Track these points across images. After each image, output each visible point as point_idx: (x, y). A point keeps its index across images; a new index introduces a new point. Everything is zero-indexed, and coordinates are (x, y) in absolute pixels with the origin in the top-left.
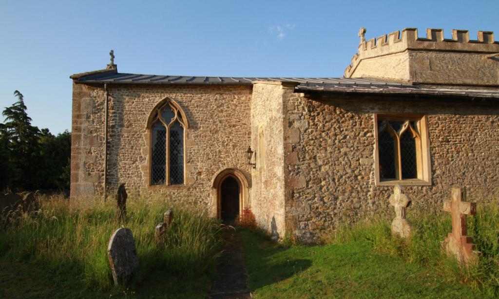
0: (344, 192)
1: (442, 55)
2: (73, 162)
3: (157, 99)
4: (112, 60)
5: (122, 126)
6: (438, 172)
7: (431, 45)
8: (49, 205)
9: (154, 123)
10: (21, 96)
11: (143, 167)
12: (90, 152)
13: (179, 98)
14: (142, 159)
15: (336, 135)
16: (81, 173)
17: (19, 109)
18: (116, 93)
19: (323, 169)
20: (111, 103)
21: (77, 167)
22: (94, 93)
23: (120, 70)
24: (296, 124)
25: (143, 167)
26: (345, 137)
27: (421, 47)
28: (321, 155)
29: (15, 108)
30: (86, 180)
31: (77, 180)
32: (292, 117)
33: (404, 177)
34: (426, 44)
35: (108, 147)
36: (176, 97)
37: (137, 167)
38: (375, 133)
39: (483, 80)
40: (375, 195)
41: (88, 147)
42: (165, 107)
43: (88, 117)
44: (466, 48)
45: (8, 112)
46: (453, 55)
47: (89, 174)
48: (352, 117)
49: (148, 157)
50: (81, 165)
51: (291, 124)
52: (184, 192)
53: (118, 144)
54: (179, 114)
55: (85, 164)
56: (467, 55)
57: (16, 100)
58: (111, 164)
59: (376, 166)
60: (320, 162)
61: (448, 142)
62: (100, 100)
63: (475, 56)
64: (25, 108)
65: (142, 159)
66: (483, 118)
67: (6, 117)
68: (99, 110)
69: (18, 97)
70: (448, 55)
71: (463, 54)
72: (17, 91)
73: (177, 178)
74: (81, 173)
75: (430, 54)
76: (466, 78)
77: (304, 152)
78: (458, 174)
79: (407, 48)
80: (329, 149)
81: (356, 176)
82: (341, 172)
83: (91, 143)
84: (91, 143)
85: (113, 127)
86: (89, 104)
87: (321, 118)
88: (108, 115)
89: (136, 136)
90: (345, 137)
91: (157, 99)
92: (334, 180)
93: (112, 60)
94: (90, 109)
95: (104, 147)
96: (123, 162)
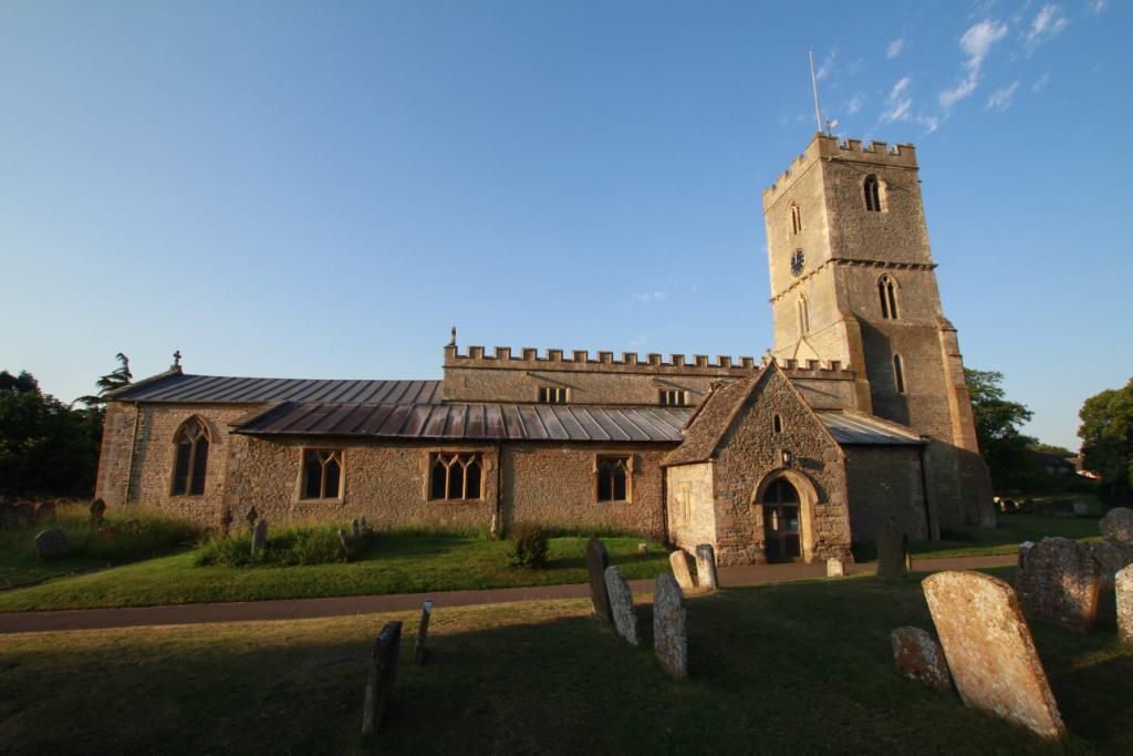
0: (270, 507)
1: (478, 371)
2: (100, 473)
3: (186, 414)
4: (177, 361)
5: (149, 440)
6: (351, 493)
7: (469, 363)
8: (106, 511)
9: (180, 437)
10: (126, 361)
11: (166, 479)
12: (117, 464)
13: (207, 415)
14: (165, 471)
15: (268, 464)
16: (107, 483)
17: (121, 378)
18: (147, 409)
19: (255, 490)
20: (142, 419)
21: (103, 478)
22: (127, 409)
23: (185, 371)
24: (238, 456)
25: (166, 479)
26: (276, 466)
27: (459, 364)
28: (254, 479)
29: (115, 376)
30: (110, 490)
31: (102, 490)
32: (235, 450)
33: (451, 497)
34: (464, 361)
35: (134, 460)
36: (202, 412)
37: (160, 479)
38: (301, 462)
39: (519, 396)
40: (294, 511)
41: (115, 459)
42: (192, 421)
43: (119, 431)
44: (506, 366)
45: (104, 382)
46: (490, 372)
47: (114, 485)
48: (284, 451)
49: (171, 469)
50: (108, 476)
51: (233, 455)
52: (203, 502)
53: (144, 457)
54: (206, 430)
55: (111, 475)
56: (506, 373)
57: (118, 365)
58: (135, 475)
59: (298, 488)
60: (253, 485)
61: (362, 469)
62: (131, 416)
63: (513, 373)
64: (130, 376)
65: (165, 471)
66: (394, 450)
67: (101, 388)
68: (131, 425)
69: (121, 361)
70: (485, 372)
71: (501, 372)
72: (120, 354)
73: (198, 489)
74: (107, 483)
75: (466, 372)
76: (501, 394)
77: (241, 475)
78: (367, 495)
79: (830, 258)
80: (262, 475)
81: (281, 496)
82: (269, 493)
83: (119, 456)
84: (119, 456)
85: (141, 441)
86: (121, 419)
87: (258, 451)
88: (137, 429)
89: (162, 449)
90: (276, 466)
91: (186, 414)
92: (262, 498)
93: (177, 361)
94: (122, 424)
95: (130, 460)
96: (147, 473)
